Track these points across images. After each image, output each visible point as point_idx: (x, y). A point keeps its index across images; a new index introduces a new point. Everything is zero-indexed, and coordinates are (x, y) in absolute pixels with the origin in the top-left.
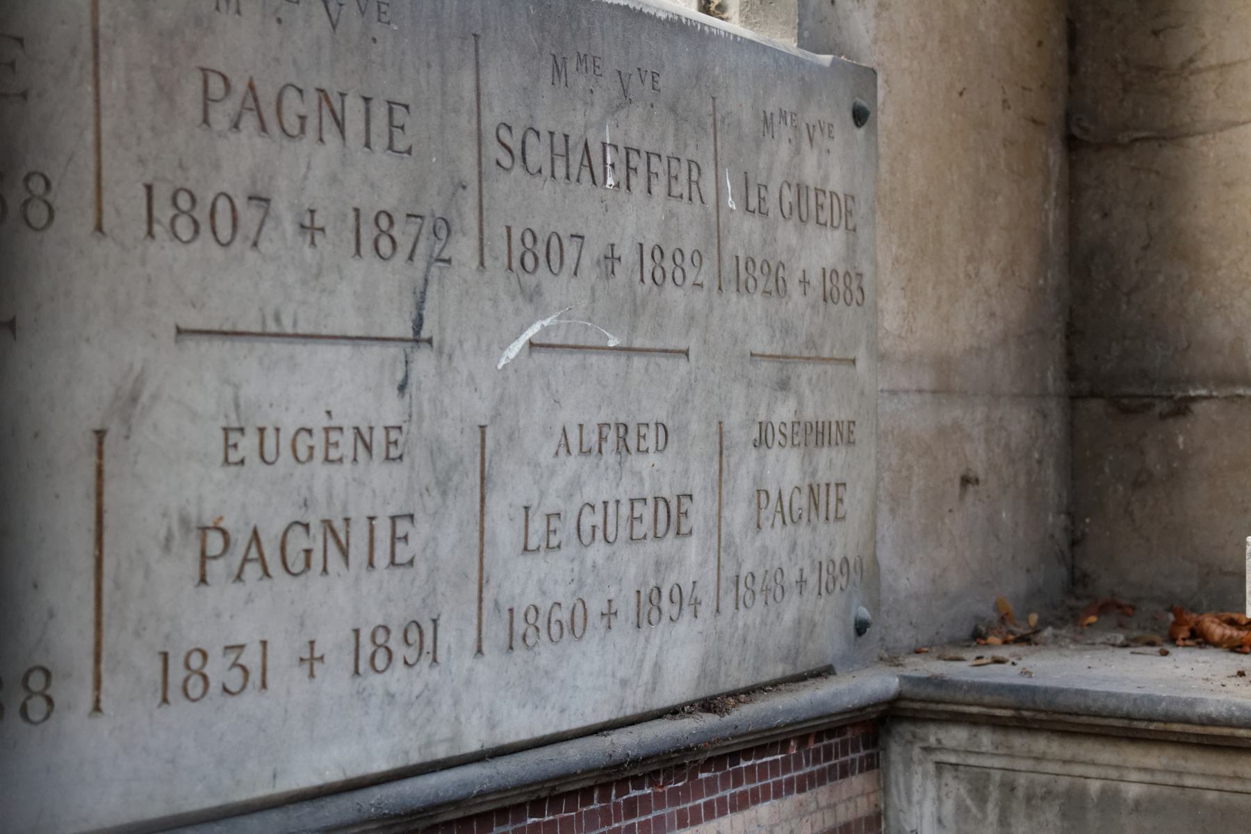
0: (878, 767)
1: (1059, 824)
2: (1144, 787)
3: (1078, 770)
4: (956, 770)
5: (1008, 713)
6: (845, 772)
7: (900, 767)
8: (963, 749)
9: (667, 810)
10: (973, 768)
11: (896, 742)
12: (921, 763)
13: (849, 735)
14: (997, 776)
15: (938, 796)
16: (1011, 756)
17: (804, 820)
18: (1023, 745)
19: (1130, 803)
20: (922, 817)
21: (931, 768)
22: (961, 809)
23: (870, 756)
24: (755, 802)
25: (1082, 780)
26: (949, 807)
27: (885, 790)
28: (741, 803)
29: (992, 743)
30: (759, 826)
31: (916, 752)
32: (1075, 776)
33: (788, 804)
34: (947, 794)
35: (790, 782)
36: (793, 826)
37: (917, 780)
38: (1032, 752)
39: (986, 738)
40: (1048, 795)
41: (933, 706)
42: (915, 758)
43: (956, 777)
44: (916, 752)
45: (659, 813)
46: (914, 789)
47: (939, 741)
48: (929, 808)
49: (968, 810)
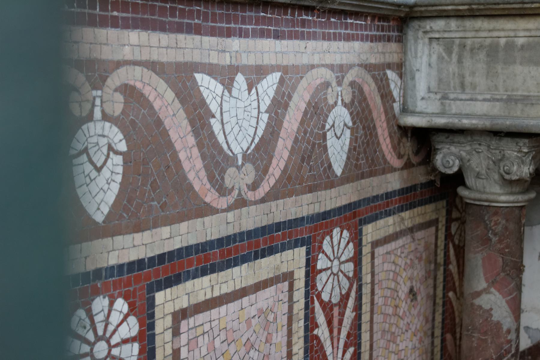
0: (402, 42)
1: (485, 59)
2: (526, 39)
3: (496, 34)
4: (438, 41)
5: (466, 7)
6: (389, 40)
7: (413, 42)
8: (442, 30)
9: (318, 30)
10: (447, 39)
11: (411, 30)
12: (422, 39)
13: (391, 23)
14: (457, 41)
15: (430, 54)
16: (465, 31)
17: (372, 55)
18: (470, 25)
19: (519, 46)
20: (421, 64)
21: (427, 40)
22: (440, 58)
23: (399, 36)
24: (353, 40)
25: (497, 39)
26: (434, 58)
27: (405, 53)
28: (348, 38)
29: (456, 26)
30: (354, 51)
31: (420, 34)
32: (494, 37)
33: (367, 45)
34: (433, 53)
35: (367, 36)
36: (368, 56)
37: (420, 47)
38: (475, 28)
39: (453, 23)
40: (481, 47)
41: (430, 8)
42: (420, 37)
43: (438, 44)
44: (420, 34)
45: (314, 30)
46: (419, 51)
47: (431, 27)
48: (425, 59)
49: (443, 58)
